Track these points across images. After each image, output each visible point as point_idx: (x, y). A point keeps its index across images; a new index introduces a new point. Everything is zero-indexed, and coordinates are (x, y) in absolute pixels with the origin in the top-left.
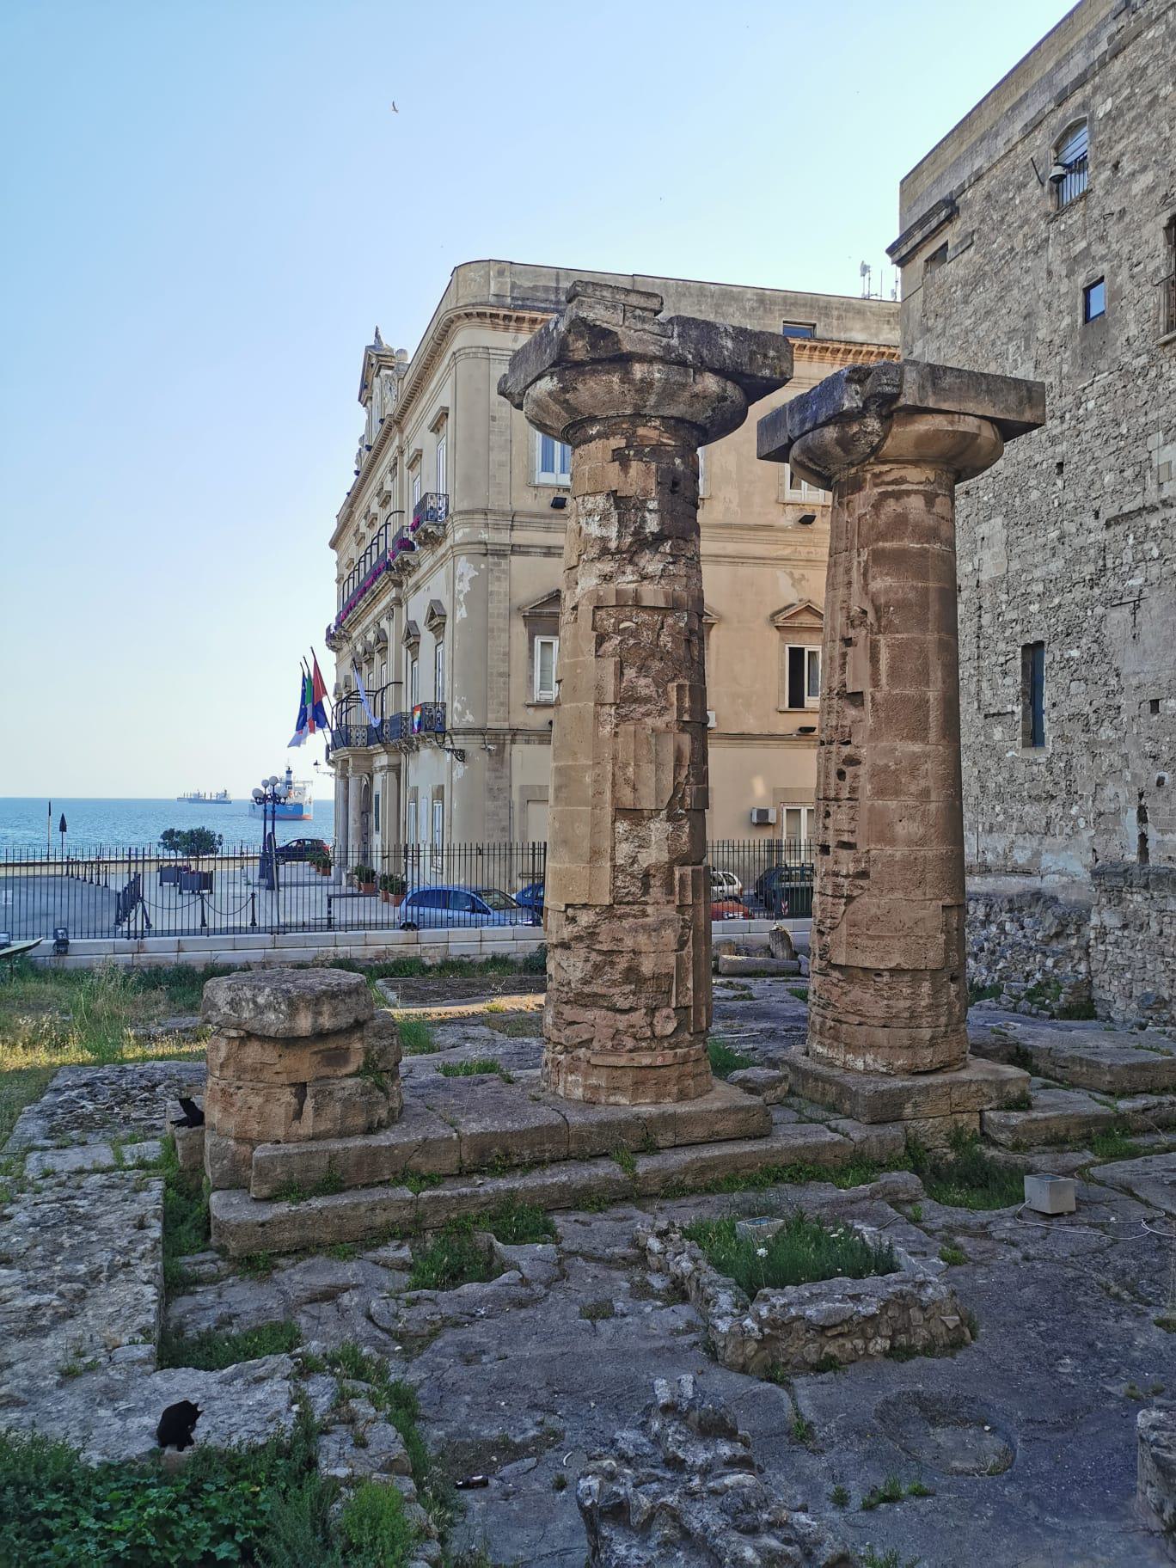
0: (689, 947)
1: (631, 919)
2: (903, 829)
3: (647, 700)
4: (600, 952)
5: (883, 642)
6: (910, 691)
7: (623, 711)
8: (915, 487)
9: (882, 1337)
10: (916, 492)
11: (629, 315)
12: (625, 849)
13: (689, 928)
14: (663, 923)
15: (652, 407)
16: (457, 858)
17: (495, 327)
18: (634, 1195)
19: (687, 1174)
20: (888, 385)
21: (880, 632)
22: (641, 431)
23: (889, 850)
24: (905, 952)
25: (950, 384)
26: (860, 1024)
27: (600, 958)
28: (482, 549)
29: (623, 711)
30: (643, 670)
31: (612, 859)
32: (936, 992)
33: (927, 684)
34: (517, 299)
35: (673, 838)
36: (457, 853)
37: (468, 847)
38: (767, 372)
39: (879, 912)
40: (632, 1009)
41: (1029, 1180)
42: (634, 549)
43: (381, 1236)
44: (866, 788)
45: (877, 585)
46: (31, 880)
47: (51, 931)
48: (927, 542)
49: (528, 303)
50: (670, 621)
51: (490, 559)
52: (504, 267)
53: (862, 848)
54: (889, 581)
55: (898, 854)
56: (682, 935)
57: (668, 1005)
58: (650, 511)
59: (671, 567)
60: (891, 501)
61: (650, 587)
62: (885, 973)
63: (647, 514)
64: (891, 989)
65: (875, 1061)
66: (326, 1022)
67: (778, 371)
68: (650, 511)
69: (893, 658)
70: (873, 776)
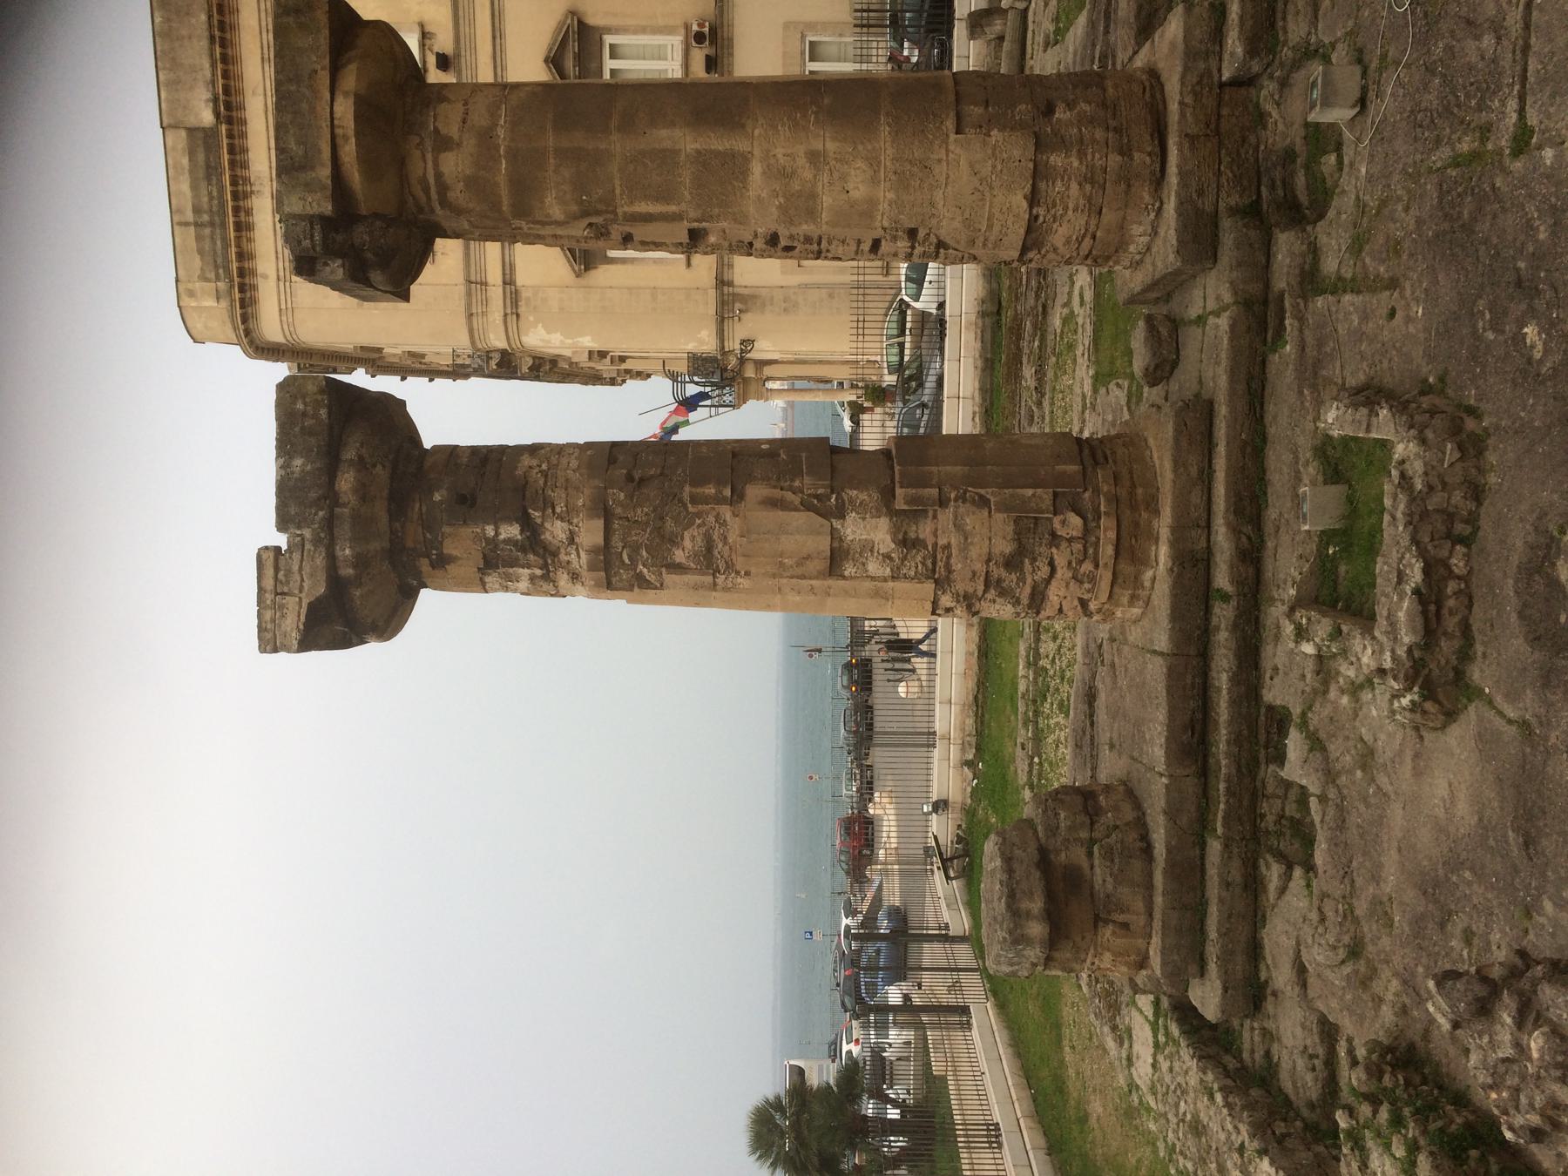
1: (953, 561)
2: (858, 188)
5: (626, 209)
6: (686, 176)
7: (722, 566)
8: (430, 164)
9: (1450, 558)
10: (436, 164)
11: (286, 590)
13: (965, 493)
14: (958, 527)
18: (1253, 446)
19: (1240, 532)
20: (312, 236)
21: (614, 212)
23: (883, 206)
25: (298, 143)
26: (1094, 237)
27: (993, 591)
28: (512, 319)
29: (722, 566)
30: (675, 541)
32: (1063, 144)
33: (676, 152)
35: (862, 508)
36: (861, 278)
37: (855, 298)
38: (323, 412)
39: (960, 219)
40: (1052, 564)
41: (1309, 120)
42: (541, 551)
44: (806, 228)
45: (557, 212)
47: (924, 817)
48: (497, 148)
49: (219, 261)
50: (619, 510)
53: (878, 233)
54: (549, 199)
55: (891, 195)
56: (973, 502)
57: (1050, 520)
59: (558, 510)
60: (451, 195)
61: (582, 535)
62: (1034, 212)
63: (502, 537)
64: (1054, 205)
65: (1140, 223)
67: (320, 397)
68: (497, 534)
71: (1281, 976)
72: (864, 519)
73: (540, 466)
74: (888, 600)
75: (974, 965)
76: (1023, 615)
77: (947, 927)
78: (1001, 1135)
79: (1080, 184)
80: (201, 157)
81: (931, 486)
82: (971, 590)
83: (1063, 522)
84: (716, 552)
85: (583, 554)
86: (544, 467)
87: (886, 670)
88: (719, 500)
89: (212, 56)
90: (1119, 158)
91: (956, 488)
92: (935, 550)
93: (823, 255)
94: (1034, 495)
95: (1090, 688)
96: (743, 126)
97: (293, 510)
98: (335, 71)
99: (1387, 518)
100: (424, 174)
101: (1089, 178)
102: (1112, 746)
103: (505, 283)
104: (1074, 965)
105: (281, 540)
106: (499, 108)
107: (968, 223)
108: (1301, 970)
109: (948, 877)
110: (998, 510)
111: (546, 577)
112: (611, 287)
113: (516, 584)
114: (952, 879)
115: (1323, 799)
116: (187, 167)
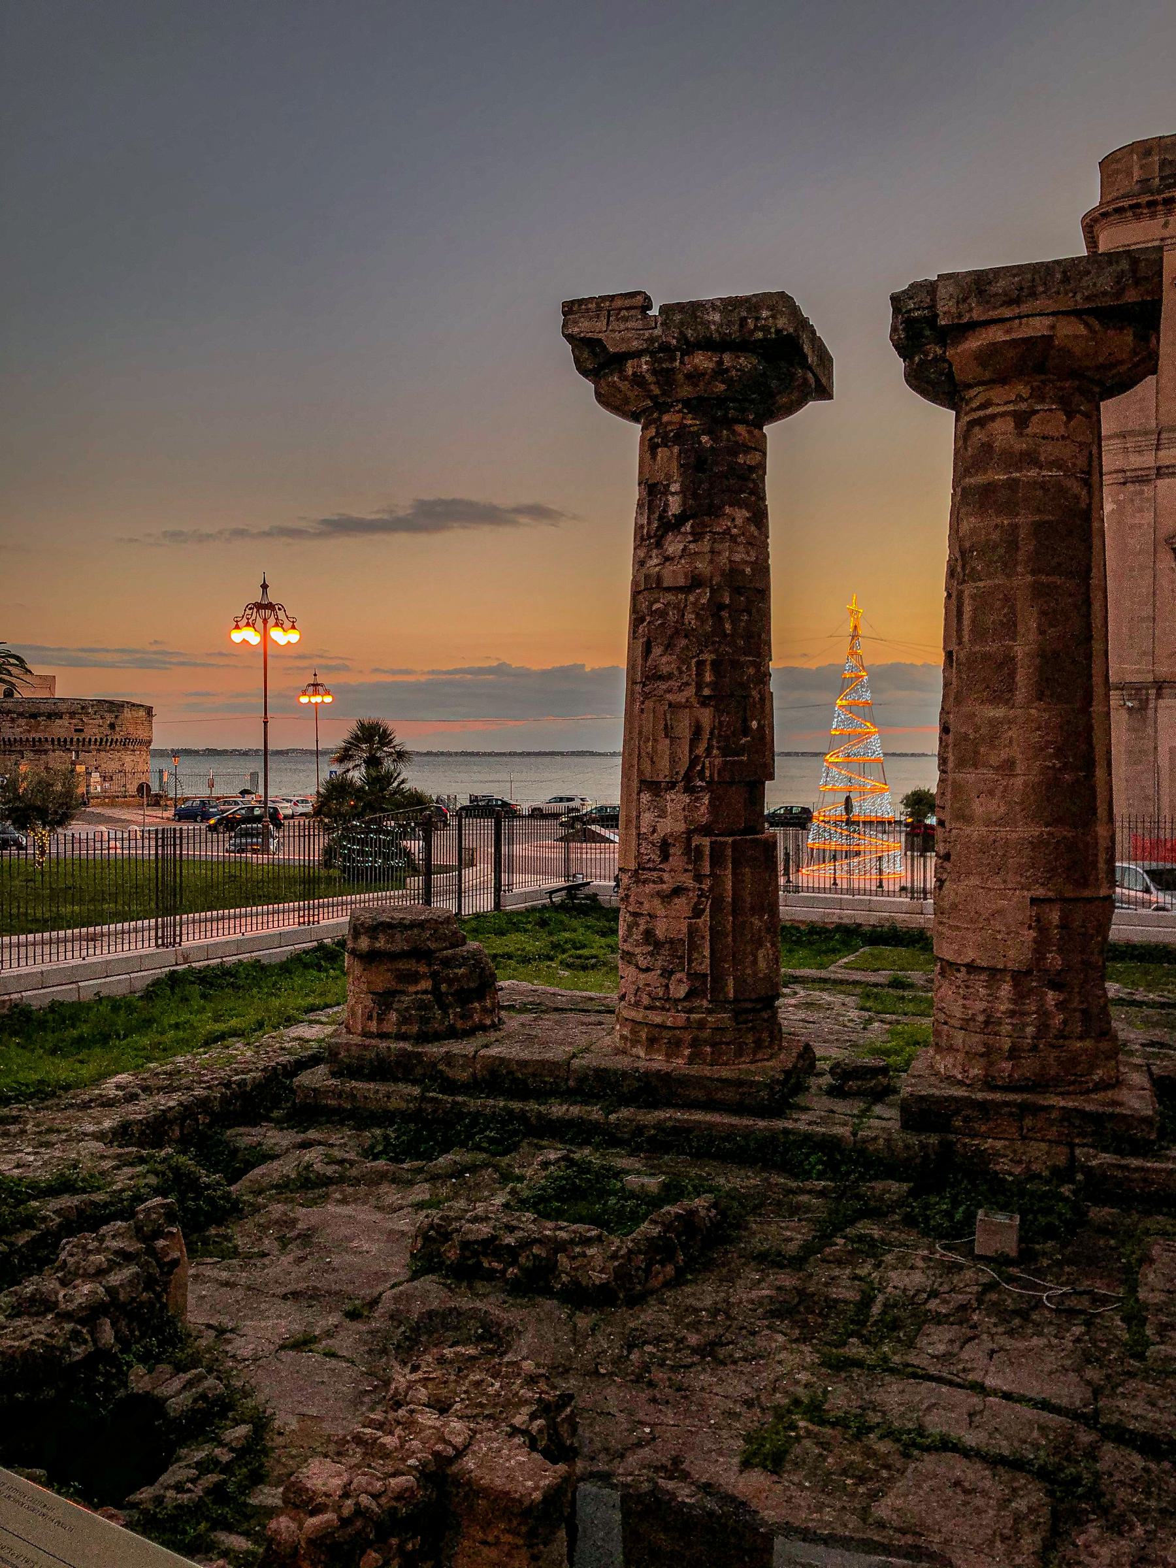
0: (706, 916)
1: (652, 885)
3: (670, 676)
6: (992, 647)
7: (646, 689)
10: (1003, 415)
12: (647, 817)
17: (1138, 217)
20: (918, 309)
21: (964, 581)
22: (665, 418)
24: (979, 946)
31: (638, 828)
35: (690, 808)
40: (647, 970)
48: (1019, 470)
50: (692, 598)
51: (1131, 488)
52: (1144, 148)
56: (698, 903)
59: (692, 546)
60: (977, 429)
63: (670, 498)
68: (673, 494)
69: (975, 610)
72: (684, 809)
73: (735, 527)
79: (984, 1010)
83: (680, 981)
84: (659, 683)
85: (657, 569)
86: (734, 531)
88: (699, 686)
90: (1007, 1047)
91: (711, 889)
94: (704, 957)
97: (678, 317)
98: (1078, 313)
103: (1159, 468)
106: (1059, 468)
110: (690, 925)
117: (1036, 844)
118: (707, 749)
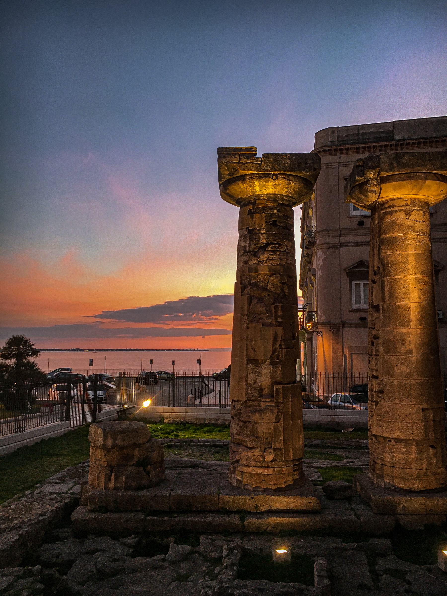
4: (243, 422)
5: (386, 281)
7: (251, 318)
8: (400, 208)
10: (400, 210)
12: (251, 377)
15: (259, 191)
16: (348, 378)
23: (392, 380)
31: (246, 381)
34: (340, 141)
43: (127, 533)
44: (381, 349)
46: (191, 383)
51: (331, 250)
52: (333, 130)
55: (396, 382)
58: (262, 234)
63: (261, 236)
66: (119, 442)
70: (384, 344)
71: (90, 544)
72: (270, 372)
74: (238, 382)
75: (85, 423)
76: (232, 436)
77: (99, 412)
78: (20, 433)
80: (383, 135)
81: (283, 399)
82: (242, 415)
87: (192, 390)
89: (420, 138)
92: (258, 401)
93: (370, 356)
94: (281, 440)
95: (198, 466)
96: (420, 325)
99: (285, 584)
100: (396, 206)
101: (406, 462)
102: (179, 474)
103: (341, 243)
104: (94, 459)
105: (259, 155)
107: (387, 413)
108: (93, 552)
109: (118, 412)
110: (275, 426)
111: (245, 252)
112: (340, 282)
113: (243, 241)
114: (118, 414)
115: (164, 560)
116: (379, 131)
117: (421, 384)
118: (280, 345)
